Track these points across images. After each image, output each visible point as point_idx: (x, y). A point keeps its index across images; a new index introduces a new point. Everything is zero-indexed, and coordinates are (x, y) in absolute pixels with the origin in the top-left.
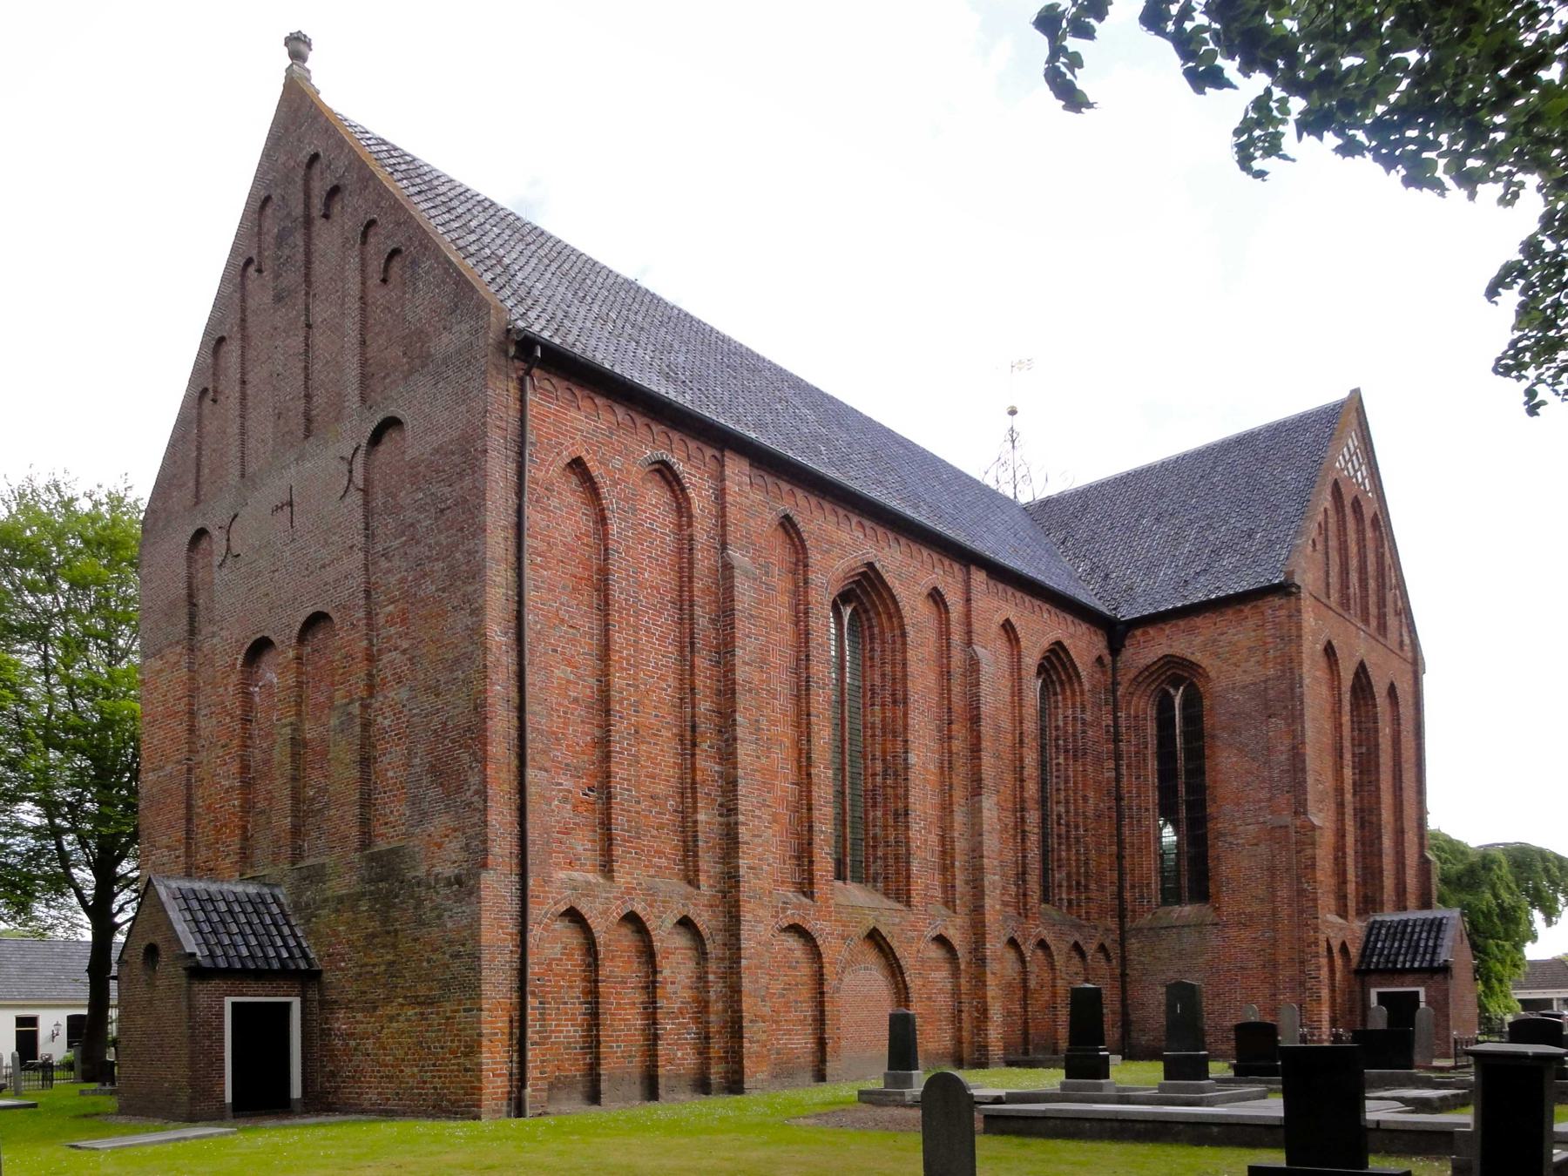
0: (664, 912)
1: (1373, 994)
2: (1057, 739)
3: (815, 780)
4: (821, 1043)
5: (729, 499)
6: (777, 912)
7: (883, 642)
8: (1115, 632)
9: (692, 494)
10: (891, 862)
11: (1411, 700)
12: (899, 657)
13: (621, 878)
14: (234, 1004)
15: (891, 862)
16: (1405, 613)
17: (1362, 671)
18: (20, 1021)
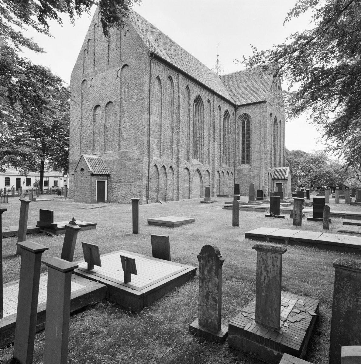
1: (275, 183)
4: (190, 191)
5: (180, 83)
7: (200, 110)
8: (236, 107)
9: (174, 82)
10: (200, 155)
12: (203, 114)
13: (162, 159)
14: (97, 181)
15: (200, 155)
18: (17, 179)
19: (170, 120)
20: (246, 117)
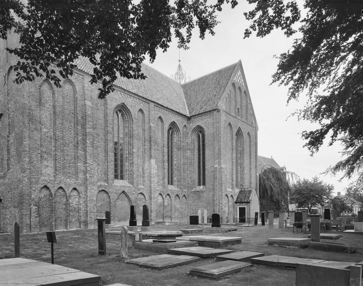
0: (69, 187)
2: (175, 145)
3: (109, 156)
6: (98, 187)
11: (254, 137)
14: (245, 208)
16: (253, 115)
17: (239, 130)
19: (73, 132)
20: (200, 130)
